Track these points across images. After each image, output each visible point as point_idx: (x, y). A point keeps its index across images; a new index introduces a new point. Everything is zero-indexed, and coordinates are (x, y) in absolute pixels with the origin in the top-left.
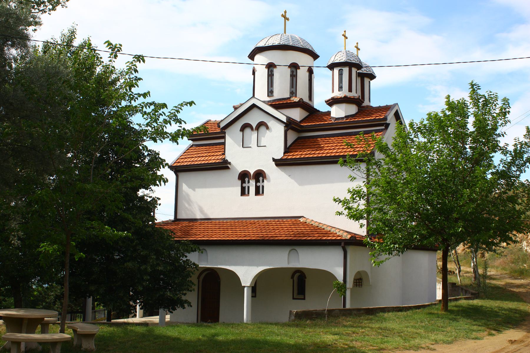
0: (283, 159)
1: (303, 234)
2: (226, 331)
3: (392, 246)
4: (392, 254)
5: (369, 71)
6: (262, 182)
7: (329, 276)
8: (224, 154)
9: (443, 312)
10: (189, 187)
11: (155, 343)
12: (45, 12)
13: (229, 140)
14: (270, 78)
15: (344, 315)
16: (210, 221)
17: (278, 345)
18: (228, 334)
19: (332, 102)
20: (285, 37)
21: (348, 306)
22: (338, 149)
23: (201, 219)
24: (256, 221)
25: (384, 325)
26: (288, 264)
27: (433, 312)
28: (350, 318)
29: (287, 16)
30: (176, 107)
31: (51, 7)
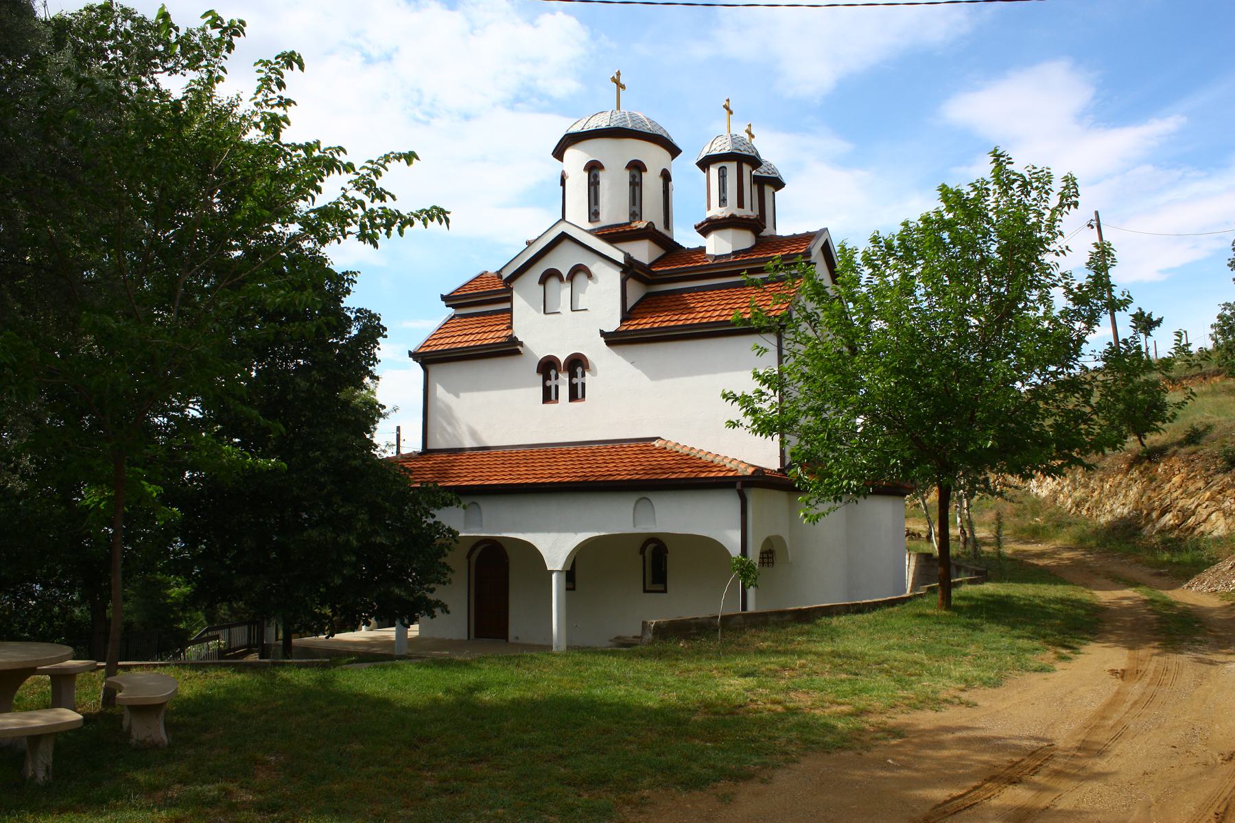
2: (502, 676)
4: (841, 501)
8: (510, 328)
10: (449, 390)
11: (328, 715)
12: (176, 72)
13: (518, 301)
15: (753, 625)
17: (622, 713)
18: (505, 684)
19: (707, 228)
21: (751, 608)
22: (723, 309)
23: (472, 449)
24: (572, 448)
25: (841, 645)
26: (634, 526)
27: (923, 612)
28: (766, 631)
29: (622, 81)
30: (371, 162)
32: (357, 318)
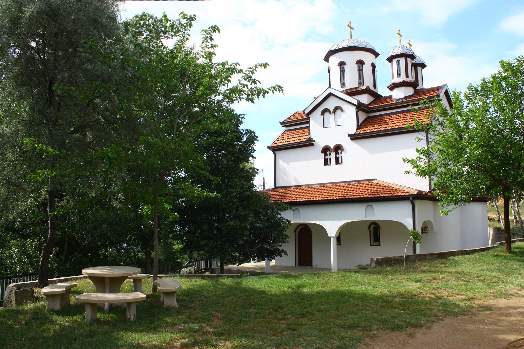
1: (376, 192)
2: (312, 282)
3: (459, 196)
4: (458, 205)
5: (421, 61)
7: (399, 226)
8: (309, 134)
9: (508, 254)
11: (240, 297)
12: (169, 38)
14: (342, 73)
16: (302, 187)
17: (364, 298)
19: (393, 87)
20: (351, 41)
21: (418, 252)
23: (295, 186)
24: (337, 184)
25: (460, 269)
26: (366, 217)
30: (250, 68)
31: (173, 34)
32: (246, 133)
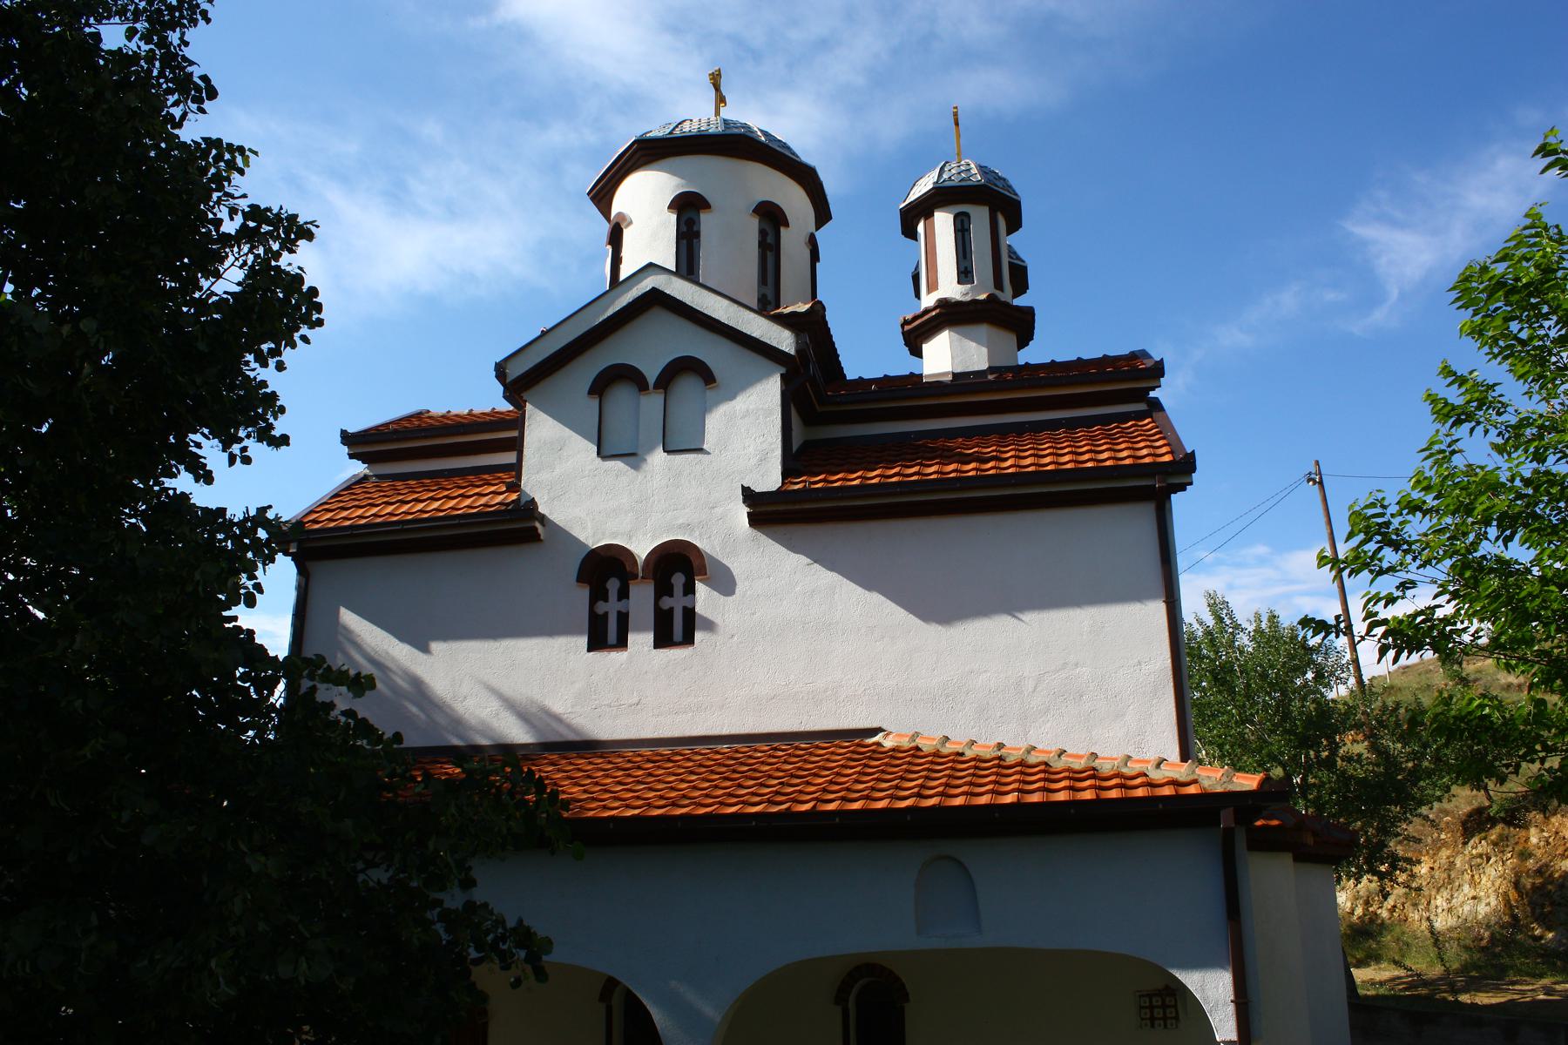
0: (781, 492)
6: (685, 594)
32: (244, 234)
